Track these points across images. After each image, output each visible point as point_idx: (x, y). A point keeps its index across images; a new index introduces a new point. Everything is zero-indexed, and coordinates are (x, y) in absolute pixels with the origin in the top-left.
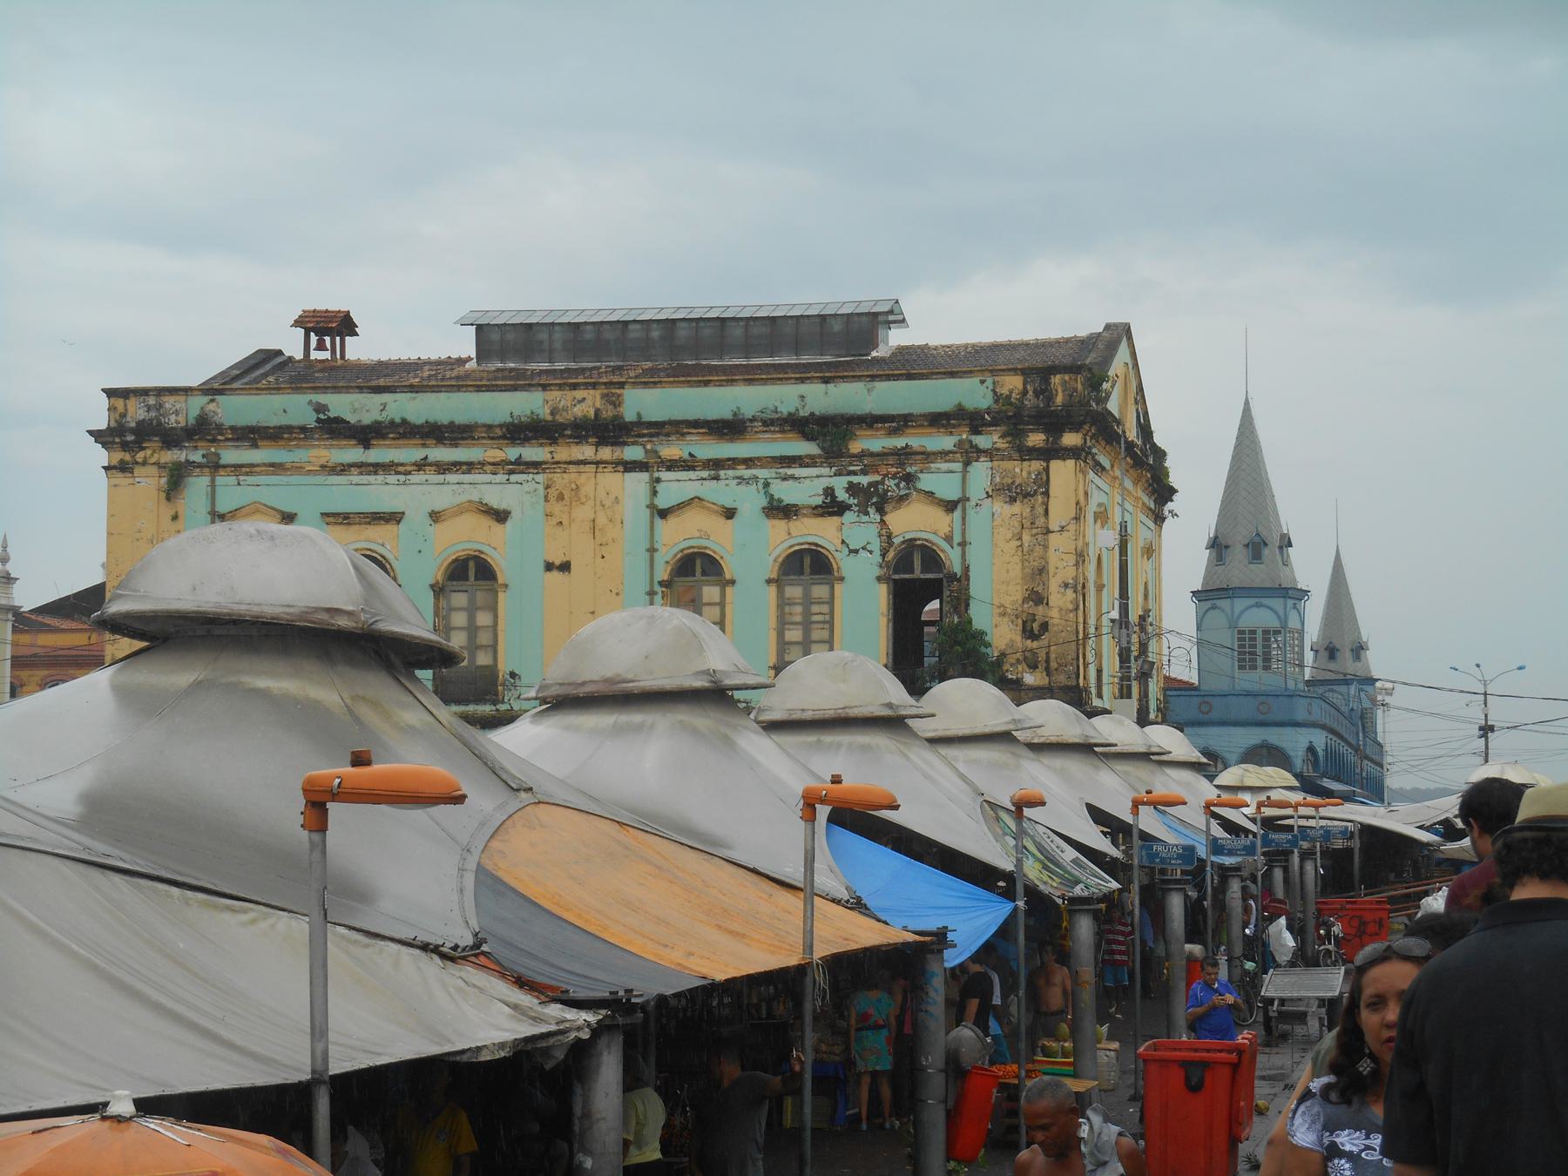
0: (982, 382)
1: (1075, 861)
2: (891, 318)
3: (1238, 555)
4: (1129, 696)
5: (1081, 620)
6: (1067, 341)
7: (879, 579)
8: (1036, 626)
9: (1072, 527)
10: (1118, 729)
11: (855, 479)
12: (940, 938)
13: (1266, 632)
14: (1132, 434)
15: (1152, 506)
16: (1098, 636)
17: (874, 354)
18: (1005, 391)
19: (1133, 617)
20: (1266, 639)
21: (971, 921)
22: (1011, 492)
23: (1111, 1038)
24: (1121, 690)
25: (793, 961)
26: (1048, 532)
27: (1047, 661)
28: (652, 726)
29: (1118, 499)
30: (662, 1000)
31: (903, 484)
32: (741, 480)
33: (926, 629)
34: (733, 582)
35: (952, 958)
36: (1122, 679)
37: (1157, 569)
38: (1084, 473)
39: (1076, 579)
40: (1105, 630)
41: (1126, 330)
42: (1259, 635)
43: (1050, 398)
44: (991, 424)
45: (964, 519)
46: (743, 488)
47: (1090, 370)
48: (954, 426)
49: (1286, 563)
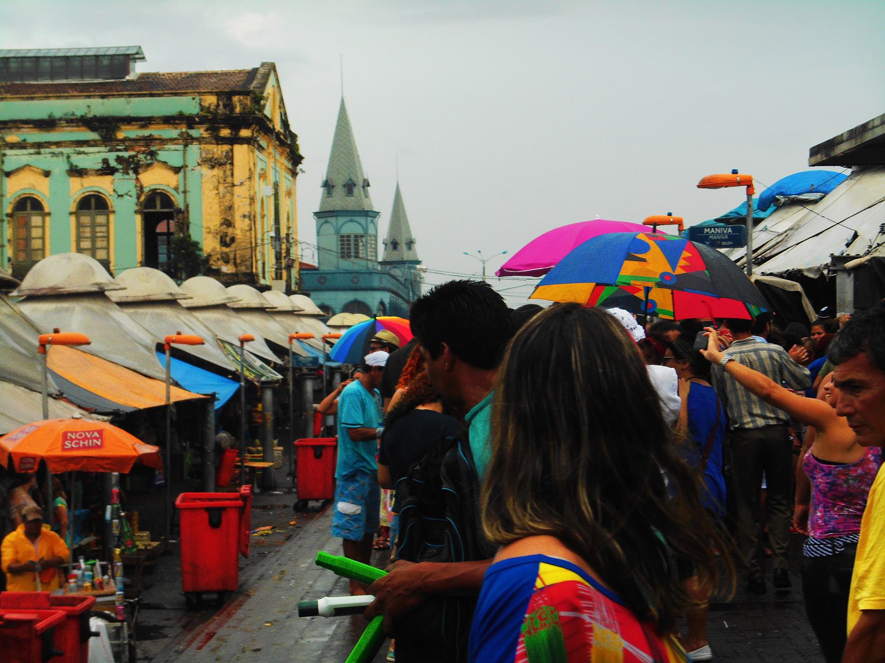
0: (194, 99)
1: (261, 366)
2: (137, 56)
3: (339, 191)
4: (281, 279)
5: (253, 236)
6: (240, 72)
7: (136, 212)
8: (228, 239)
9: (247, 183)
10: (276, 298)
11: (121, 154)
12: (213, 397)
13: (356, 236)
14: (278, 127)
15: (290, 166)
16: (263, 245)
17: (128, 78)
18: (206, 104)
19: (283, 234)
20: (356, 241)
21: (225, 391)
22: (213, 163)
23: (279, 445)
24: (276, 274)
25: (163, 403)
26: (233, 185)
27: (235, 259)
28: (73, 309)
29: (272, 165)
30: (127, 413)
31: (149, 157)
32: (54, 154)
33: (159, 237)
34: (49, 214)
35: (218, 405)
36: (277, 269)
37: (294, 204)
38: (253, 152)
39: (250, 212)
40: (266, 242)
41: (272, 67)
42: (352, 239)
43: (232, 109)
44: (198, 123)
45: (185, 178)
46: (55, 159)
47: (254, 93)
48: (178, 124)
49: (367, 197)
